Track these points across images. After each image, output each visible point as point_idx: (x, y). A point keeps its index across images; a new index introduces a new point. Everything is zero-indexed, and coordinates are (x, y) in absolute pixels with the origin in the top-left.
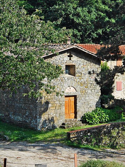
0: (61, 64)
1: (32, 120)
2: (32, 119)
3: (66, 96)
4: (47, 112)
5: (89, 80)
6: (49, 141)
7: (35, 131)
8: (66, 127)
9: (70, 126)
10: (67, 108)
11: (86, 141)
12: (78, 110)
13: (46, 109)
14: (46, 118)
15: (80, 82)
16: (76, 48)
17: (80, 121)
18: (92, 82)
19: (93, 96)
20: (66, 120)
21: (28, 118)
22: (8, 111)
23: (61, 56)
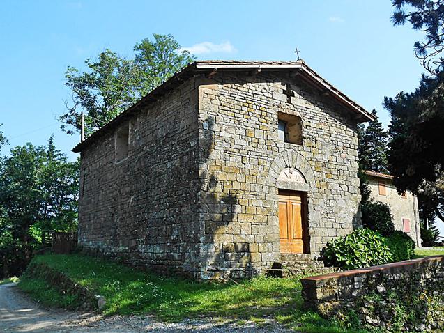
0: (266, 107)
1: (185, 251)
3: (282, 192)
4: (229, 226)
5: (334, 159)
6: (231, 314)
7: (192, 281)
8: (286, 272)
9: (296, 271)
10: (285, 222)
11: (377, 315)
12: (311, 230)
13: (228, 218)
14: (225, 244)
15: (315, 160)
17: (319, 259)
18: (340, 167)
20: (282, 256)
21: (176, 247)
22: (135, 236)
23: (267, 88)
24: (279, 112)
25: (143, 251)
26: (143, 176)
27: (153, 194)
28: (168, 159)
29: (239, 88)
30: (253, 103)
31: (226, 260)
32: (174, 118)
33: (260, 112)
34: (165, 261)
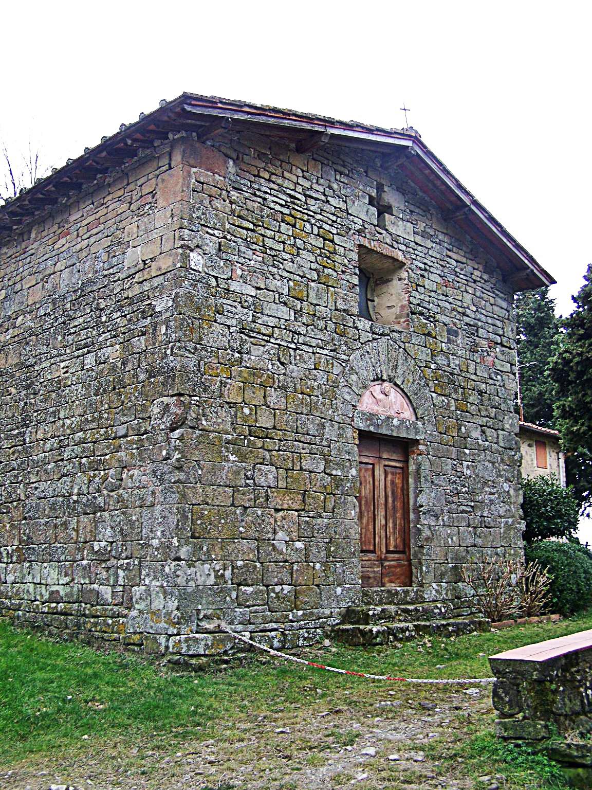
0: (335, 231)
16: (418, 155)
19: (493, 463)
24: (360, 246)
26: (13, 390)
27: (40, 435)
28: (86, 346)
29: (274, 178)
30: (306, 217)
31: (240, 605)
32: (107, 242)
33: (320, 243)
34: (75, 606)
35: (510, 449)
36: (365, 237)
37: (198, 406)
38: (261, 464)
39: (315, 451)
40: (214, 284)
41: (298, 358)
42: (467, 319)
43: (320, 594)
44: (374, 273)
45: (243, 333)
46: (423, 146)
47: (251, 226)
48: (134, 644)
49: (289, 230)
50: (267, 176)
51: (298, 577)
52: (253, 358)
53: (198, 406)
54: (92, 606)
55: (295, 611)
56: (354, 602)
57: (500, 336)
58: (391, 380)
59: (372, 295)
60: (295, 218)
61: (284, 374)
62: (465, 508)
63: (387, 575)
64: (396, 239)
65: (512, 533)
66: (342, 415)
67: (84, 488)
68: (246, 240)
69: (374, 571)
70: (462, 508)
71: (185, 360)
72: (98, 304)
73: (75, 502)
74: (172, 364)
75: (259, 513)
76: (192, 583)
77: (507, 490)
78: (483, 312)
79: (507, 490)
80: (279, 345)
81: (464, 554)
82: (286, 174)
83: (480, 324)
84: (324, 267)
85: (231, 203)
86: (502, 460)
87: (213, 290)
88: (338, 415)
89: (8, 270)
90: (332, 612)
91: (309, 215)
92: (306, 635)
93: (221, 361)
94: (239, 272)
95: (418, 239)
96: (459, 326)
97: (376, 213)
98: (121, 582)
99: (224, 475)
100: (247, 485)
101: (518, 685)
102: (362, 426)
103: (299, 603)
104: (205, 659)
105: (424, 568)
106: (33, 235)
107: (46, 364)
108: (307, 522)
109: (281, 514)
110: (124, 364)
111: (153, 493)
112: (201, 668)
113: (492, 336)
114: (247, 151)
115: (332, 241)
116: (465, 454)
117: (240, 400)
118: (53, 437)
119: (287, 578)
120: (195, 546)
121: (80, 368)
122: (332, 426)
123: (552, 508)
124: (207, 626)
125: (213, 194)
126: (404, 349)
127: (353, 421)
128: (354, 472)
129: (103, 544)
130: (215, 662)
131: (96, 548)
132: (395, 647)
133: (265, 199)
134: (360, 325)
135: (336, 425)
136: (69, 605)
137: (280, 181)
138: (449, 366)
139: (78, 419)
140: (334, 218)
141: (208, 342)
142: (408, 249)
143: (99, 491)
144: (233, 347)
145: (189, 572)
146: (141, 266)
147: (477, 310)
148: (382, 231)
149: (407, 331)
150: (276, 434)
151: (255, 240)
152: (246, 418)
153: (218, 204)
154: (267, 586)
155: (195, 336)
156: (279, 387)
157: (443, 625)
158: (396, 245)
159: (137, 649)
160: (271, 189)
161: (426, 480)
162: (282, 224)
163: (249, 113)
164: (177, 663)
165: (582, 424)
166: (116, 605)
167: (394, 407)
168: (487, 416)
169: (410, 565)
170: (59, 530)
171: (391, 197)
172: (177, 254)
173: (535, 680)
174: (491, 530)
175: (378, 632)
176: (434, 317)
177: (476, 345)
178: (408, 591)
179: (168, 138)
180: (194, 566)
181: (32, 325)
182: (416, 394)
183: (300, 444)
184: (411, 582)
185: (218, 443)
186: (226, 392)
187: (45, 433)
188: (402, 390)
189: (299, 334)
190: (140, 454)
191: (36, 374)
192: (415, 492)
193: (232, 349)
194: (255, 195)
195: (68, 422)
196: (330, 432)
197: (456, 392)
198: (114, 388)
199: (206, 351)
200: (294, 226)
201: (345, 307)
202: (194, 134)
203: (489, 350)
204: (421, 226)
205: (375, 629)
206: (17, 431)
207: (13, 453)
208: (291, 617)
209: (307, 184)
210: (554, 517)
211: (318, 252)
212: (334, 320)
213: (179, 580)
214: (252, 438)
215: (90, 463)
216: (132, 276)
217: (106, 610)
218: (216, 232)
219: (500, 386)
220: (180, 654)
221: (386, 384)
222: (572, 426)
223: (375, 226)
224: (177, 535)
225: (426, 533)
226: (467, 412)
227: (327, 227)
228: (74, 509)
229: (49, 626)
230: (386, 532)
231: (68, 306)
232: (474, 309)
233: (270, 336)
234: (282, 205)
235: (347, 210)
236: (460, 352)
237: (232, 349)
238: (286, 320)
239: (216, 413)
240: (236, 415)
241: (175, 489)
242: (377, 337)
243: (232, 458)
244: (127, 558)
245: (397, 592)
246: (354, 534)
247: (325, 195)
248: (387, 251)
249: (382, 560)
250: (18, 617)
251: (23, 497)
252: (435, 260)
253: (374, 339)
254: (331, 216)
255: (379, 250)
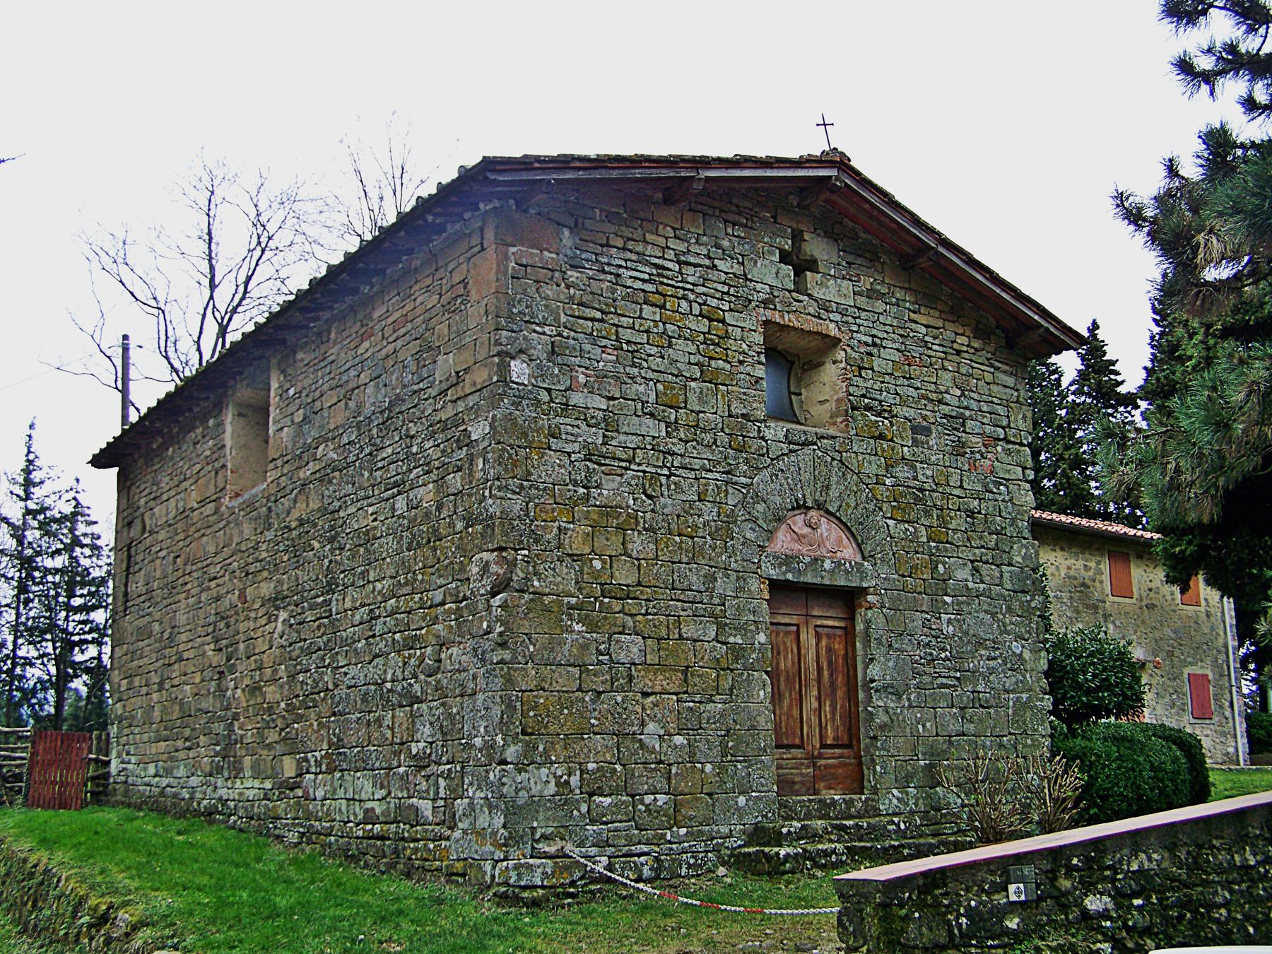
1: (456, 792)
2: (463, 773)
19: (993, 615)
21: (428, 777)
22: (293, 746)
24: (767, 323)
25: (320, 794)
26: (316, 545)
28: (396, 485)
29: (630, 245)
31: (593, 822)
32: (414, 347)
33: (703, 326)
35: (1023, 592)
36: (775, 309)
37: (527, 562)
38: (620, 633)
39: (702, 612)
40: (547, 398)
41: (673, 487)
42: (945, 409)
43: (713, 805)
44: (792, 357)
45: (590, 460)
46: (855, 174)
47: (598, 315)
48: (457, 874)
49: (655, 313)
50: (620, 243)
51: (678, 783)
52: (605, 492)
53: (527, 562)
54: (412, 826)
55: (675, 829)
56: (766, 816)
57: (1003, 428)
58: (819, 506)
59: (799, 386)
60: (665, 296)
61: (653, 511)
62: (944, 681)
63: (822, 779)
64: (825, 306)
65: (1028, 714)
66: (743, 560)
67: (398, 672)
68: (591, 334)
69: (802, 774)
70: (940, 680)
71: (506, 504)
72: (408, 430)
73: (389, 691)
74: (491, 510)
75: (619, 699)
76: (523, 793)
77: (1018, 652)
78: (973, 395)
79: (1018, 652)
80: (644, 472)
81: (945, 747)
82: (649, 237)
83: (967, 413)
84: (711, 358)
85: (568, 287)
86: (1009, 609)
87: (545, 407)
88: (736, 561)
89: (306, 383)
90: (732, 831)
91: (684, 289)
92: (692, 861)
93: (558, 500)
94: (582, 379)
95: (862, 301)
96: (932, 420)
97: (792, 274)
98: (442, 794)
99: (565, 652)
100: (600, 663)
101: (861, 911)
102: (774, 573)
103: (679, 818)
104: (541, 891)
105: (878, 768)
106: (333, 335)
107: (352, 510)
108: (690, 709)
109: (651, 698)
110: (439, 509)
111: (474, 677)
112: (535, 903)
113: (988, 429)
114: (590, 213)
115: (723, 321)
116: (945, 603)
117: (587, 550)
118: (362, 605)
119: (661, 784)
120: (527, 744)
121: (390, 515)
122: (728, 576)
123: (1095, 676)
124: (547, 849)
125: (541, 277)
126: (841, 461)
127: (760, 567)
128: (762, 638)
129: (422, 745)
130: (557, 895)
131: (414, 751)
132: (814, 876)
133: (618, 275)
134: (768, 434)
135: (733, 576)
136: (386, 827)
137: (640, 248)
138: (915, 478)
139: (390, 582)
140: (725, 289)
141: (540, 477)
142: (845, 319)
143: (415, 676)
144: (576, 481)
145: (519, 779)
146: (454, 380)
147: (963, 394)
148: (801, 297)
149: (845, 435)
150: (642, 592)
151: (604, 333)
152: (596, 574)
153: (549, 291)
154: (633, 796)
155: (520, 471)
156: (645, 529)
157: (893, 846)
158: (824, 314)
159: (460, 880)
160: (626, 261)
161: (879, 643)
162: (644, 306)
163: (579, 169)
164: (504, 896)
165: (1190, 543)
166: (438, 824)
167: (827, 543)
168: (983, 547)
169: (860, 764)
170: (372, 729)
171: (816, 247)
172: (492, 363)
173: (879, 904)
174: (992, 710)
175: (788, 855)
176: (890, 411)
177: (963, 445)
178: (852, 801)
179: (478, 209)
180: (526, 771)
181: (335, 456)
182: (861, 523)
183: (679, 604)
184: (863, 788)
185: (556, 609)
186: (567, 541)
187: (354, 600)
188: (839, 519)
189: (673, 454)
190: (459, 626)
191: (341, 522)
192: (864, 662)
193: (575, 484)
194: (604, 272)
195: (379, 586)
196: (723, 586)
197: (927, 514)
198: (429, 541)
199: (537, 488)
200: (663, 307)
201: (744, 411)
202: (512, 202)
203: (984, 450)
204: (866, 282)
205: (782, 852)
206: (322, 598)
207: (319, 628)
208: (668, 838)
209: (682, 247)
210: (1098, 689)
211: (701, 338)
212: (727, 431)
213: (505, 790)
214: (606, 600)
215: (404, 640)
216: (443, 393)
217: (426, 831)
218: (547, 329)
219: (1003, 501)
220: (509, 885)
221: (813, 513)
222: (1173, 546)
223: (790, 291)
224: (501, 730)
225: (881, 718)
226: (947, 542)
227: (714, 302)
228: (388, 701)
229: (364, 854)
230: (818, 717)
231: (375, 431)
232: (958, 393)
233: (630, 462)
234: (644, 281)
235: (745, 274)
236: (933, 458)
237: (575, 484)
238: (654, 438)
239: (554, 569)
240: (581, 571)
241: (498, 671)
242: (796, 447)
243: (578, 627)
244: (448, 763)
245: (834, 802)
246: (765, 721)
247: (710, 258)
248: (811, 324)
249: (813, 757)
250: (330, 843)
251: (331, 687)
252: (889, 329)
253: (791, 451)
254: (720, 287)
255: (797, 324)
